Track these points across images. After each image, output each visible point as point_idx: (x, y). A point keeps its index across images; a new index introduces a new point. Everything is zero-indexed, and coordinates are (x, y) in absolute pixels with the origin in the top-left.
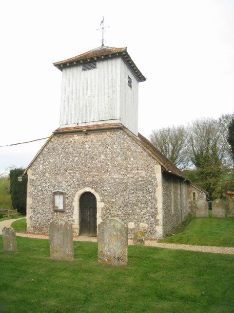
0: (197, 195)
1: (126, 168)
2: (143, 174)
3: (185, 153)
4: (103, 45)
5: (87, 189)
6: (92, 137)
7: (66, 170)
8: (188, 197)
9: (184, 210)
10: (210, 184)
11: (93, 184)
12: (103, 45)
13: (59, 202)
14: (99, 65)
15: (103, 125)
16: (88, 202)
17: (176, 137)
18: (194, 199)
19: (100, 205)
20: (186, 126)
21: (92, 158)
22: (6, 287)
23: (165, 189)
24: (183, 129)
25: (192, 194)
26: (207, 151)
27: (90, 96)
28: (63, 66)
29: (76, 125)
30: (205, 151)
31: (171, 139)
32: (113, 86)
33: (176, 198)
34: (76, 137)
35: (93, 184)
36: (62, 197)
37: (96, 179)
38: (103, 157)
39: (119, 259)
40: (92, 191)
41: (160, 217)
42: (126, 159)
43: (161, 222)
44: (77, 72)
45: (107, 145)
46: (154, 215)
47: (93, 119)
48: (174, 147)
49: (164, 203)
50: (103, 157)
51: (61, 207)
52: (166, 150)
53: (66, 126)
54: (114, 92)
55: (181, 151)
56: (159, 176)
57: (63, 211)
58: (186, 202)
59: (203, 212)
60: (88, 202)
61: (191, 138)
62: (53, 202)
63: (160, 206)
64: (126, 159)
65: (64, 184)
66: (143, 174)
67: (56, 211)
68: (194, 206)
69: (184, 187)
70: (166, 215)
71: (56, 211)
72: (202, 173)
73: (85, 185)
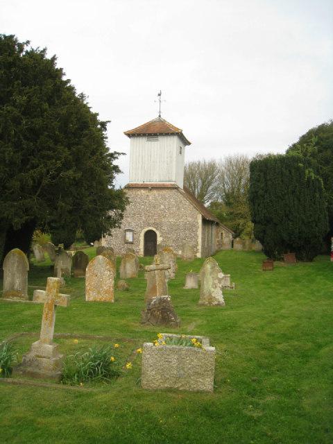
0: (224, 235)
1: (179, 215)
2: (190, 219)
3: (216, 189)
4: (160, 116)
5: (150, 228)
6: (155, 192)
7: (134, 214)
8: (217, 237)
9: (213, 247)
10: (239, 225)
11: (155, 225)
12: (160, 116)
13: (129, 236)
14: (160, 138)
15: (163, 185)
16: (150, 237)
17: (207, 172)
18: (222, 238)
19: (159, 239)
20: (217, 162)
21: (154, 207)
22: (2, 325)
23: (203, 229)
24: (214, 164)
25: (220, 234)
26: (239, 189)
27: (154, 162)
28: (131, 135)
29: (142, 183)
30: (236, 190)
31: (200, 174)
32: (171, 157)
33: (208, 236)
34: (143, 191)
35: (155, 225)
36: (131, 233)
37: (158, 221)
38: (162, 207)
39: (190, 258)
40: (154, 230)
41: (200, 247)
42: (179, 209)
43: (200, 251)
44: (142, 142)
45: (165, 199)
46: (196, 246)
47: (155, 180)
48: (203, 183)
49: (202, 238)
50: (162, 207)
51: (131, 240)
52: (194, 185)
53: (135, 183)
54: (171, 162)
55: (210, 188)
56: (200, 221)
57: (132, 243)
58: (215, 241)
59: (228, 247)
60: (150, 237)
61: (223, 175)
62: (125, 236)
63: (200, 240)
64: (179, 209)
65: (133, 224)
66: (190, 219)
67: (127, 243)
68: (221, 244)
69: (214, 227)
70: (203, 246)
71: (127, 243)
72: (231, 213)
73: (149, 225)
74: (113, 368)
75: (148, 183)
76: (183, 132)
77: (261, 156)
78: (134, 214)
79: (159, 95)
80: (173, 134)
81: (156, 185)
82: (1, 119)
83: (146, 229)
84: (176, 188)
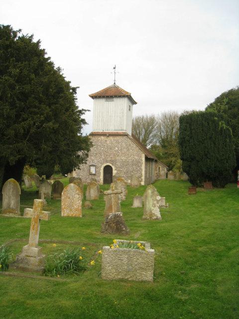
0: (161, 169)
1: (128, 155)
2: (136, 157)
3: (155, 136)
4: (115, 83)
5: (108, 164)
6: (111, 138)
7: (96, 154)
8: (156, 170)
9: (153, 178)
10: (171, 161)
11: (111, 161)
12: (115, 83)
13: (93, 170)
14: (115, 99)
15: (117, 133)
16: (108, 170)
17: (148, 123)
18: (159, 171)
19: (114, 172)
20: (156, 116)
21: (111, 149)
22: (1, 233)
23: (146, 165)
24: (154, 118)
25: (158, 168)
26: (171, 136)
27: (110, 116)
28: (94, 97)
29: (102, 131)
30: (169, 136)
31: (144, 125)
32: (123, 113)
33: (149, 169)
34: (102, 137)
35: (111, 161)
36: (94, 167)
37: (113, 159)
38: (117, 148)
39: (136, 186)
40: (111, 165)
41: (143, 178)
42: (128, 150)
43: (144, 180)
44: (102, 102)
45: (119, 143)
46: (140, 177)
47: (111, 129)
48: (146, 131)
49: (145, 171)
50: (117, 148)
51: (94, 172)
52: (140, 133)
53: (97, 131)
54: (123, 116)
55: (151, 135)
56: (144, 159)
57: (95, 175)
58: (154, 173)
59: (164, 177)
60: (108, 170)
61: (160, 126)
62: (90, 170)
63: (143, 173)
64: (128, 150)
65: (96, 161)
66: (136, 157)
67: (91, 174)
68: (158, 175)
69: (154, 163)
70: (146, 177)
71: (91, 175)
72: (166, 153)
73: (107, 162)
74: (81, 265)
75: (106, 131)
76: (131, 95)
78: (96, 154)
79: (114, 68)
80: (124, 96)
81: (112, 133)
82: (1, 86)
83: (105, 165)
84: (126, 135)
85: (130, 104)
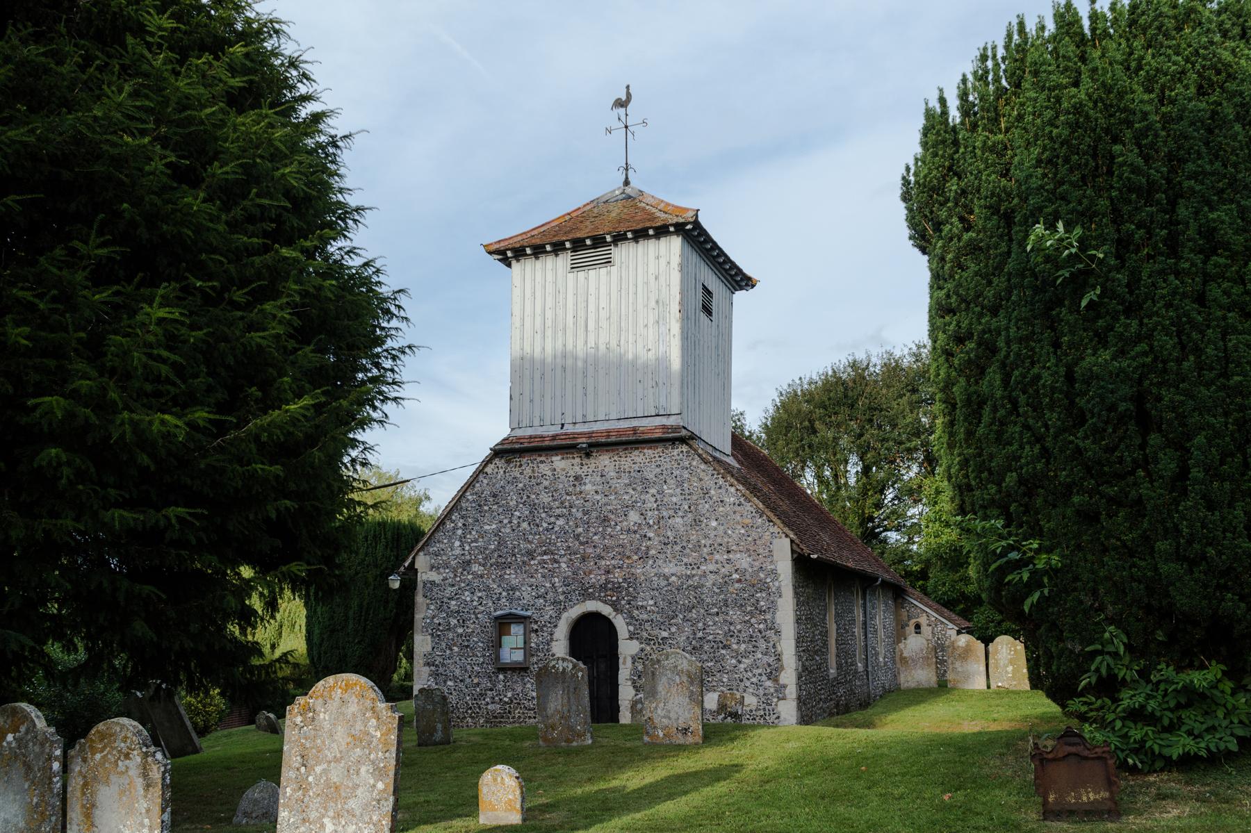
2: (744, 561)
4: (627, 183)
5: (592, 606)
6: (604, 461)
12: (627, 183)
14: (623, 253)
29: (556, 430)
34: (558, 462)
35: (607, 590)
37: (617, 576)
40: (606, 610)
41: (789, 677)
43: (792, 691)
50: (634, 517)
63: (788, 647)
65: (526, 594)
73: (586, 595)
74: (151, 789)
75: (580, 428)
76: (703, 220)
77: (930, 704)
78: (531, 554)
79: (621, 104)
80: (662, 231)
81: (608, 433)
82: (329, 827)
83: (575, 612)
84: (683, 440)
85: (715, 284)
